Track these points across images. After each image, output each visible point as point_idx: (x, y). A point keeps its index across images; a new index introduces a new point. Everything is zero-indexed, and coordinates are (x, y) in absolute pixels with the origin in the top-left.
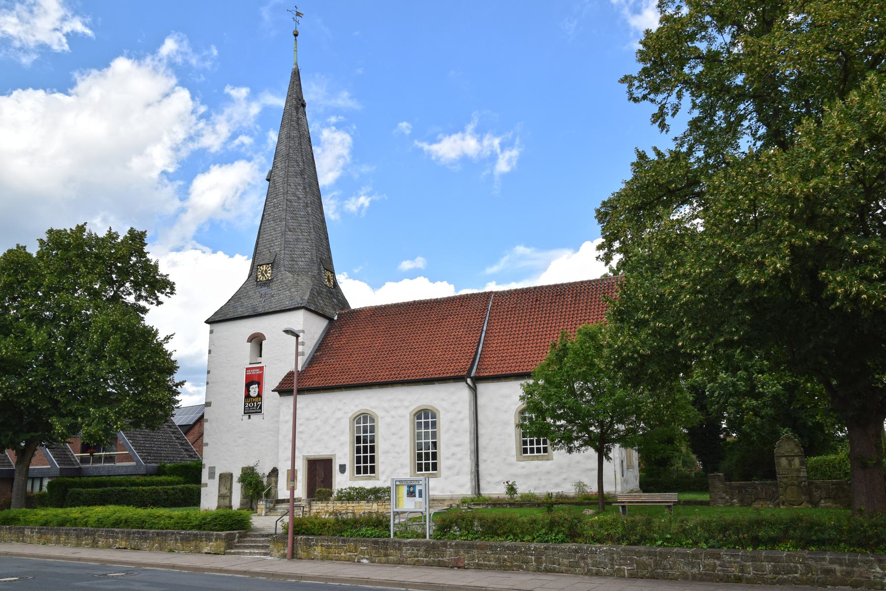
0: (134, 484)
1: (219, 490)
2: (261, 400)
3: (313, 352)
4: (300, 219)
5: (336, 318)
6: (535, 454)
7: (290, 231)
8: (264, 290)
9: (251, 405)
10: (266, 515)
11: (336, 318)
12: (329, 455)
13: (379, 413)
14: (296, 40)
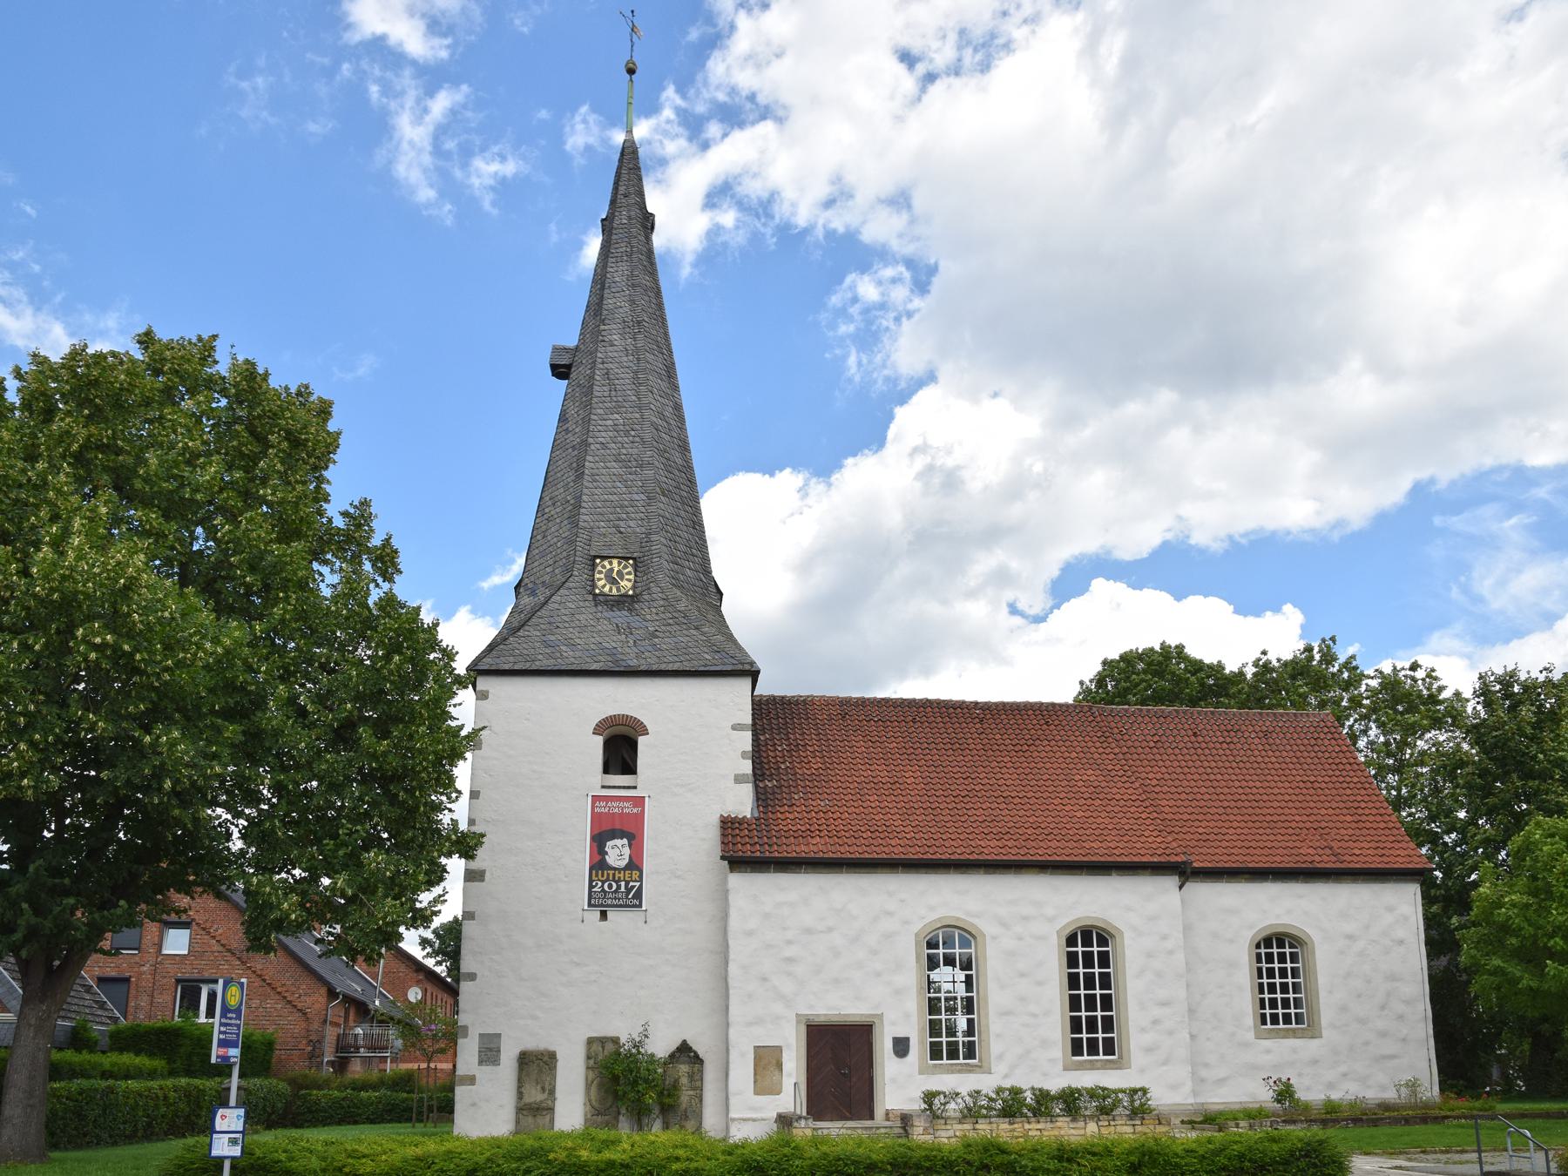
2: (641, 877)
6: (1281, 1026)
9: (610, 886)
13: (985, 926)
14: (631, 80)
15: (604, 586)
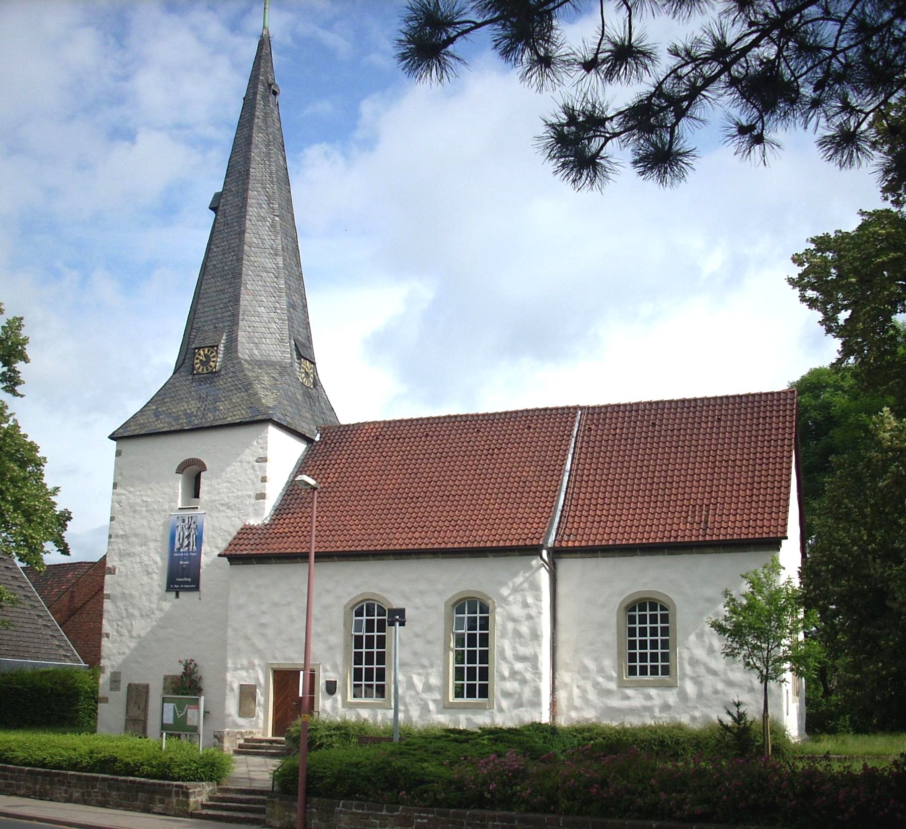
1: (127, 710)
5: (317, 439)
8: (204, 389)
11: (317, 439)
15: (199, 368)
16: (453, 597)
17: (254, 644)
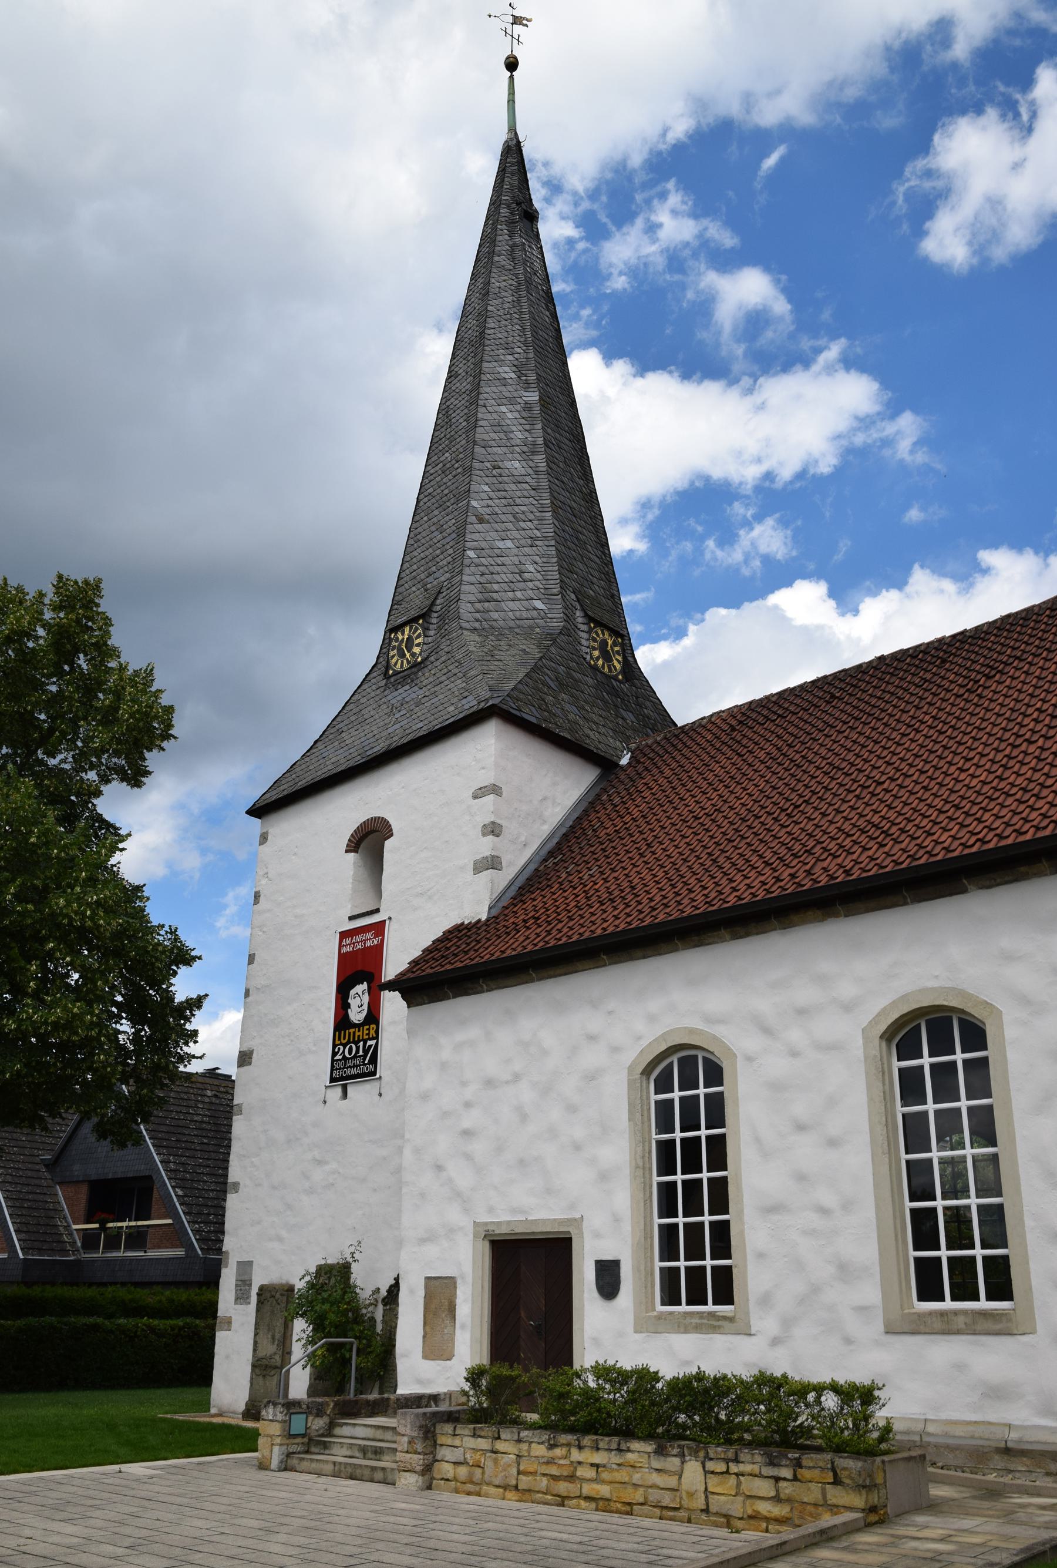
0: (137, 1310)
1: (255, 1343)
3: (539, 859)
4: (513, 487)
7: (481, 521)
8: (404, 692)
10: (285, 1468)
12: (562, 1222)
16: (883, 1012)
17: (450, 1180)
